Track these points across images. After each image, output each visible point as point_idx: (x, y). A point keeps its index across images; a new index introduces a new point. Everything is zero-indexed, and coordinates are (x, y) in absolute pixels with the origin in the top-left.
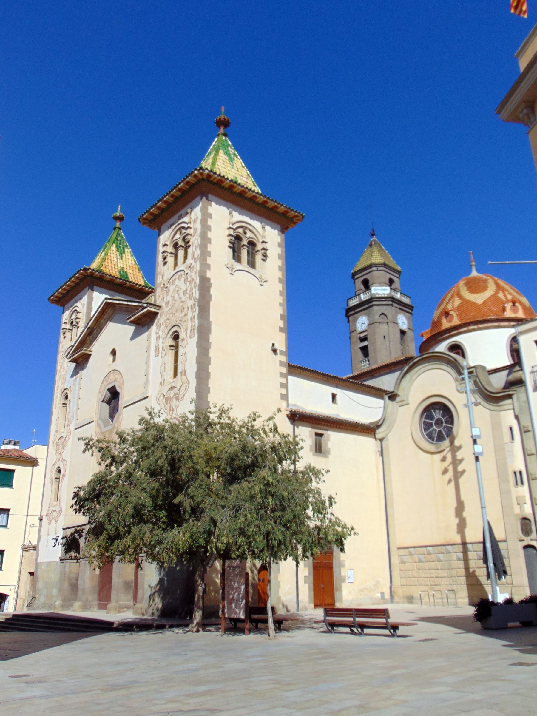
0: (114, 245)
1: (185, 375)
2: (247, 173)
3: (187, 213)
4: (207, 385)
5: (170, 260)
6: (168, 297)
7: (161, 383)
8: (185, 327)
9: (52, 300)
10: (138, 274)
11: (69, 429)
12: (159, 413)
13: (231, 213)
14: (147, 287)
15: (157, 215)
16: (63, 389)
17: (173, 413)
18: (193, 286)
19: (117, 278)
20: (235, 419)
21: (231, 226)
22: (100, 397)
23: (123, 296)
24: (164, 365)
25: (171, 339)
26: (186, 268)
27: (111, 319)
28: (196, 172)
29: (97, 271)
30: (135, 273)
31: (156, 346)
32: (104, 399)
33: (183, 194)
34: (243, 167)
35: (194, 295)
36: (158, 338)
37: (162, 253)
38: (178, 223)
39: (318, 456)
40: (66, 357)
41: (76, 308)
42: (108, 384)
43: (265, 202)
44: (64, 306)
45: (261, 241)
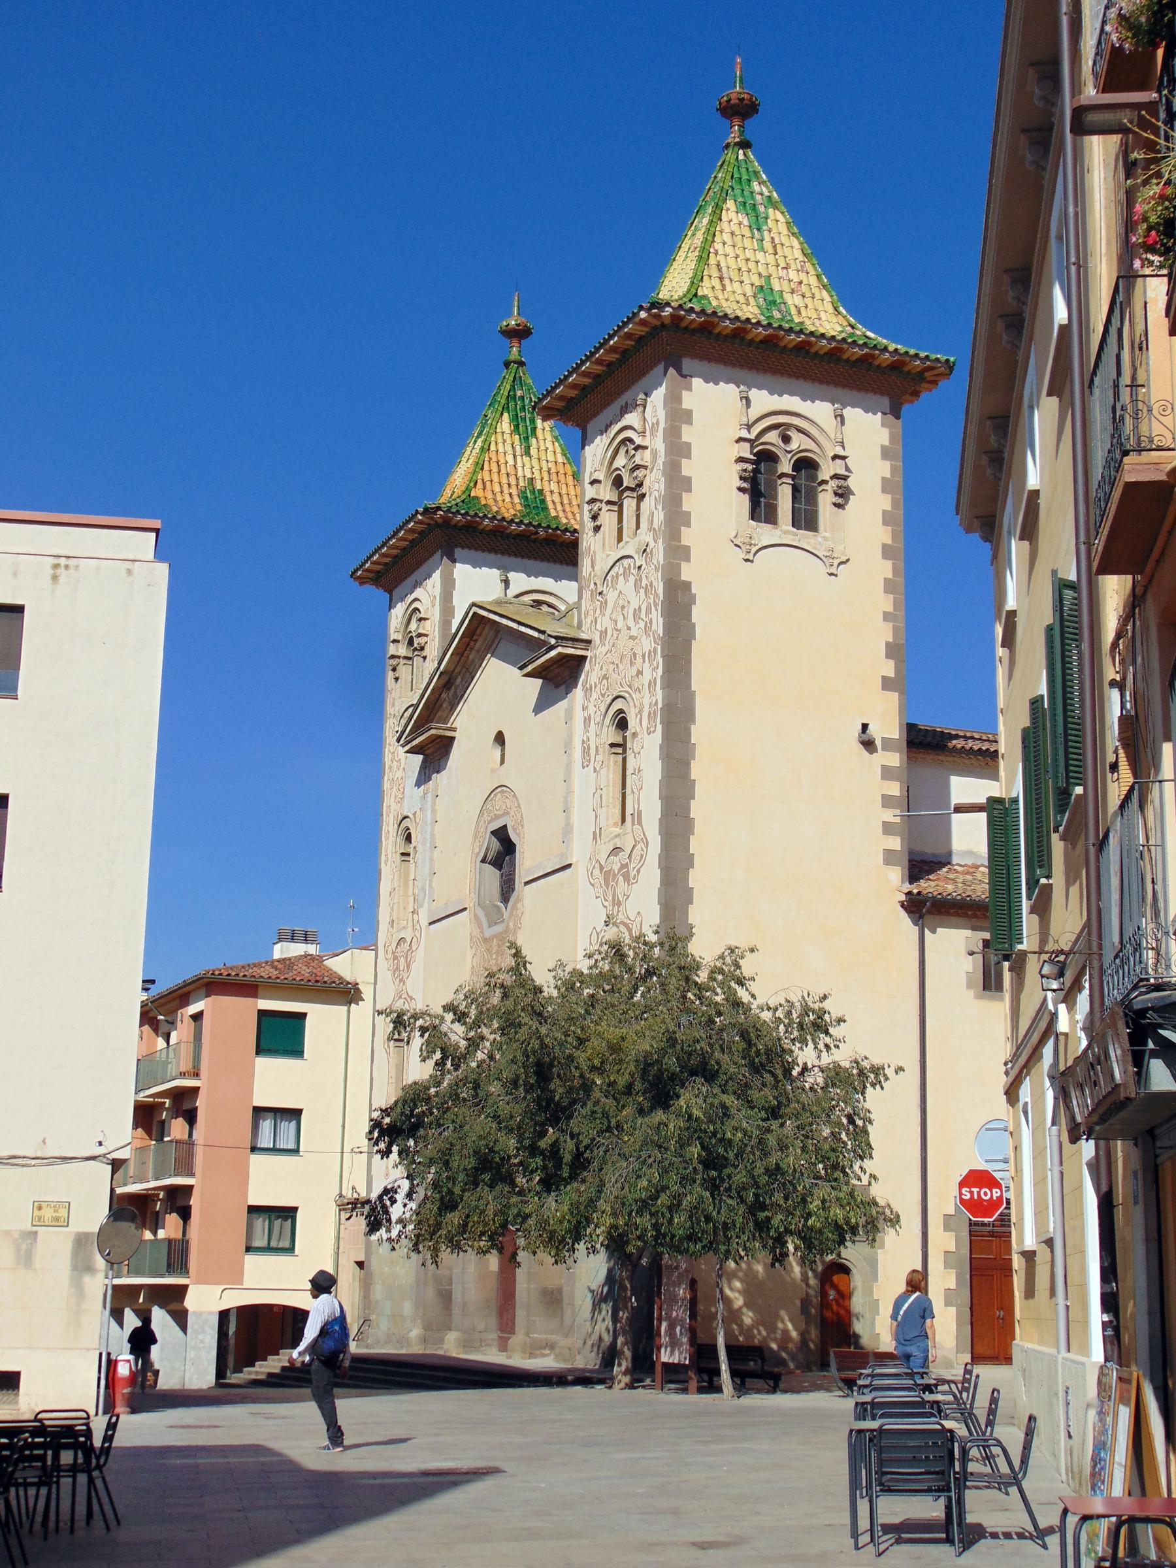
0: (506, 415)
1: (640, 823)
5: (608, 519)
8: (637, 704)
9: (359, 578)
11: (418, 921)
16: (400, 818)
17: (618, 912)
21: (744, 434)
27: (493, 647)
28: (643, 315)
30: (564, 491)
31: (583, 742)
32: (485, 857)
35: (654, 627)
36: (587, 721)
39: (991, 998)
40: (398, 741)
41: (415, 605)
44: (390, 593)
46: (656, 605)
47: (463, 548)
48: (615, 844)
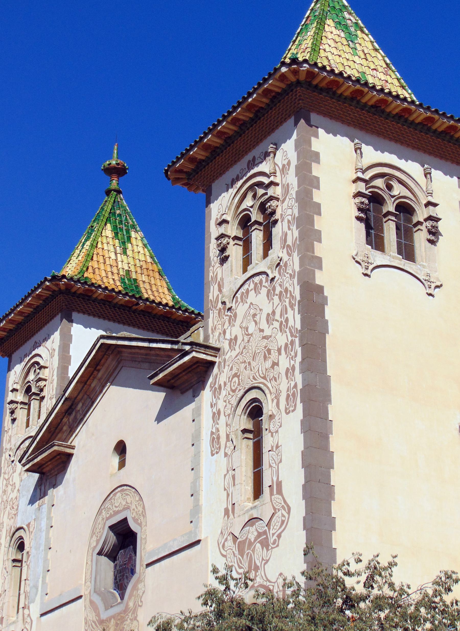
0: (109, 225)
1: (280, 492)
2: (385, 61)
3: (267, 154)
4: (329, 512)
6: (233, 329)
7: (227, 512)
10: (159, 283)
11: (29, 615)
12: (246, 578)
13: (357, 149)
14: (179, 309)
15: (203, 161)
16: (13, 530)
18: (287, 304)
19: (120, 292)
20: (405, 588)
21: (360, 175)
22: (95, 544)
23: (136, 330)
24: (231, 472)
25: (244, 418)
26: (270, 268)
28: (284, 69)
29: (78, 281)
30: (153, 282)
31: (212, 433)
33: (256, 115)
34: (376, 50)
35: (291, 323)
36: (216, 416)
37: (217, 239)
38: (249, 175)
40: (20, 461)
42: (111, 516)
43: (430, 120)
44: (10, 356)
45: (424, 202)
46: (292, 306)
47: (79, 312)
48: (252, 515)
